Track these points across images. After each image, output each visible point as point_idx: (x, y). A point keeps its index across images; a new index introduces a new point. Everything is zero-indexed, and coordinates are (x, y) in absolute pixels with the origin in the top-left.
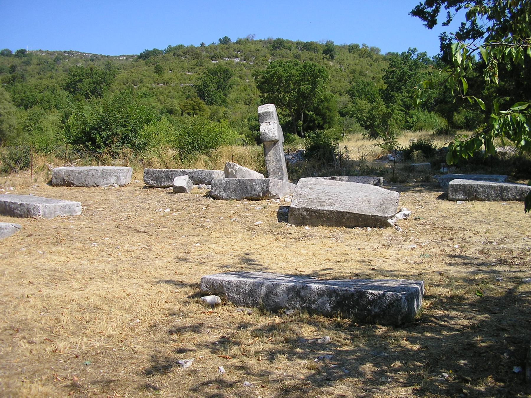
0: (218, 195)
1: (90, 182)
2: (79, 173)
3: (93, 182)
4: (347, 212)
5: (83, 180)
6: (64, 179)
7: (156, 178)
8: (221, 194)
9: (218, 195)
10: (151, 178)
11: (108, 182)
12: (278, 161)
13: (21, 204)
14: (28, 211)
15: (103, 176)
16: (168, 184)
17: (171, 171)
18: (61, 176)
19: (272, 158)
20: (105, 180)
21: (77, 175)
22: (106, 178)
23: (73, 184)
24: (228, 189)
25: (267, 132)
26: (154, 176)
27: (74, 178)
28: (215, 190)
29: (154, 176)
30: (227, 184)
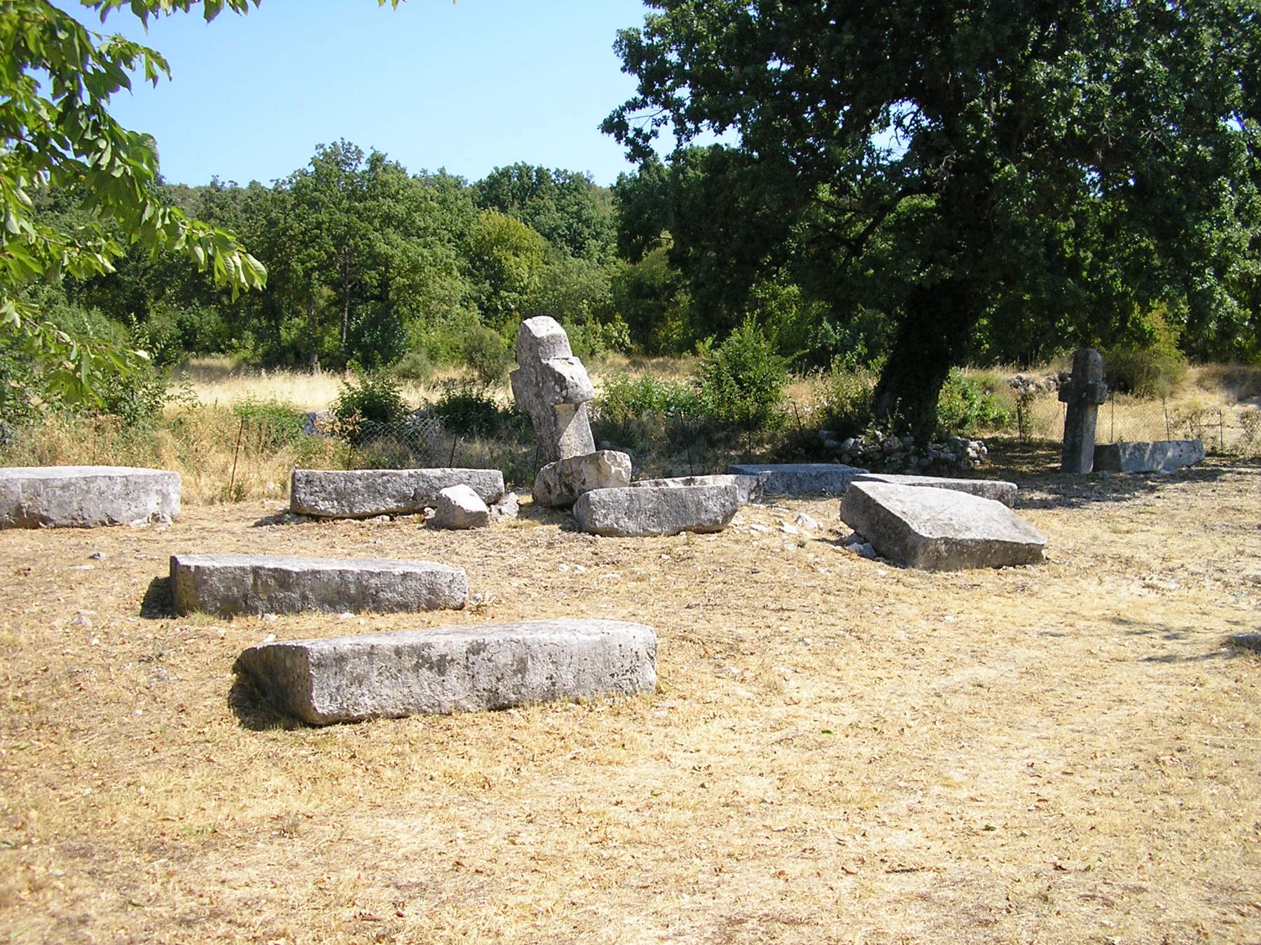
0: (616, 526)
1: (95, 512)
2: (63, 488)
3: (102, 513)
4: (997, 541)
5: (75, 506)
6: (20, 508)
7: (338, 494)
8: (621, 522)
9: (616, 526)
10: (323, 495)
11: (141, 510)
12: (585, 445)
13: (405, 576)
14: (432, 591)
15: (128, 494)
16: (374, 508)
17: (383, 475)
18: (14, 498)
19: (573, 439)
20: (133, 504)
21: (58, 492)
22: (133, 500)
23: (46, 520)
24: (638, 511)
25: (576, 380)
26: (330, 488)
27: (49, 502)
28: (605, 516)
29: (330, 488)
30: (631, 500)
